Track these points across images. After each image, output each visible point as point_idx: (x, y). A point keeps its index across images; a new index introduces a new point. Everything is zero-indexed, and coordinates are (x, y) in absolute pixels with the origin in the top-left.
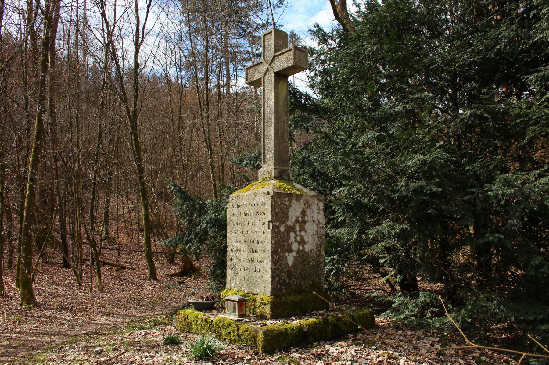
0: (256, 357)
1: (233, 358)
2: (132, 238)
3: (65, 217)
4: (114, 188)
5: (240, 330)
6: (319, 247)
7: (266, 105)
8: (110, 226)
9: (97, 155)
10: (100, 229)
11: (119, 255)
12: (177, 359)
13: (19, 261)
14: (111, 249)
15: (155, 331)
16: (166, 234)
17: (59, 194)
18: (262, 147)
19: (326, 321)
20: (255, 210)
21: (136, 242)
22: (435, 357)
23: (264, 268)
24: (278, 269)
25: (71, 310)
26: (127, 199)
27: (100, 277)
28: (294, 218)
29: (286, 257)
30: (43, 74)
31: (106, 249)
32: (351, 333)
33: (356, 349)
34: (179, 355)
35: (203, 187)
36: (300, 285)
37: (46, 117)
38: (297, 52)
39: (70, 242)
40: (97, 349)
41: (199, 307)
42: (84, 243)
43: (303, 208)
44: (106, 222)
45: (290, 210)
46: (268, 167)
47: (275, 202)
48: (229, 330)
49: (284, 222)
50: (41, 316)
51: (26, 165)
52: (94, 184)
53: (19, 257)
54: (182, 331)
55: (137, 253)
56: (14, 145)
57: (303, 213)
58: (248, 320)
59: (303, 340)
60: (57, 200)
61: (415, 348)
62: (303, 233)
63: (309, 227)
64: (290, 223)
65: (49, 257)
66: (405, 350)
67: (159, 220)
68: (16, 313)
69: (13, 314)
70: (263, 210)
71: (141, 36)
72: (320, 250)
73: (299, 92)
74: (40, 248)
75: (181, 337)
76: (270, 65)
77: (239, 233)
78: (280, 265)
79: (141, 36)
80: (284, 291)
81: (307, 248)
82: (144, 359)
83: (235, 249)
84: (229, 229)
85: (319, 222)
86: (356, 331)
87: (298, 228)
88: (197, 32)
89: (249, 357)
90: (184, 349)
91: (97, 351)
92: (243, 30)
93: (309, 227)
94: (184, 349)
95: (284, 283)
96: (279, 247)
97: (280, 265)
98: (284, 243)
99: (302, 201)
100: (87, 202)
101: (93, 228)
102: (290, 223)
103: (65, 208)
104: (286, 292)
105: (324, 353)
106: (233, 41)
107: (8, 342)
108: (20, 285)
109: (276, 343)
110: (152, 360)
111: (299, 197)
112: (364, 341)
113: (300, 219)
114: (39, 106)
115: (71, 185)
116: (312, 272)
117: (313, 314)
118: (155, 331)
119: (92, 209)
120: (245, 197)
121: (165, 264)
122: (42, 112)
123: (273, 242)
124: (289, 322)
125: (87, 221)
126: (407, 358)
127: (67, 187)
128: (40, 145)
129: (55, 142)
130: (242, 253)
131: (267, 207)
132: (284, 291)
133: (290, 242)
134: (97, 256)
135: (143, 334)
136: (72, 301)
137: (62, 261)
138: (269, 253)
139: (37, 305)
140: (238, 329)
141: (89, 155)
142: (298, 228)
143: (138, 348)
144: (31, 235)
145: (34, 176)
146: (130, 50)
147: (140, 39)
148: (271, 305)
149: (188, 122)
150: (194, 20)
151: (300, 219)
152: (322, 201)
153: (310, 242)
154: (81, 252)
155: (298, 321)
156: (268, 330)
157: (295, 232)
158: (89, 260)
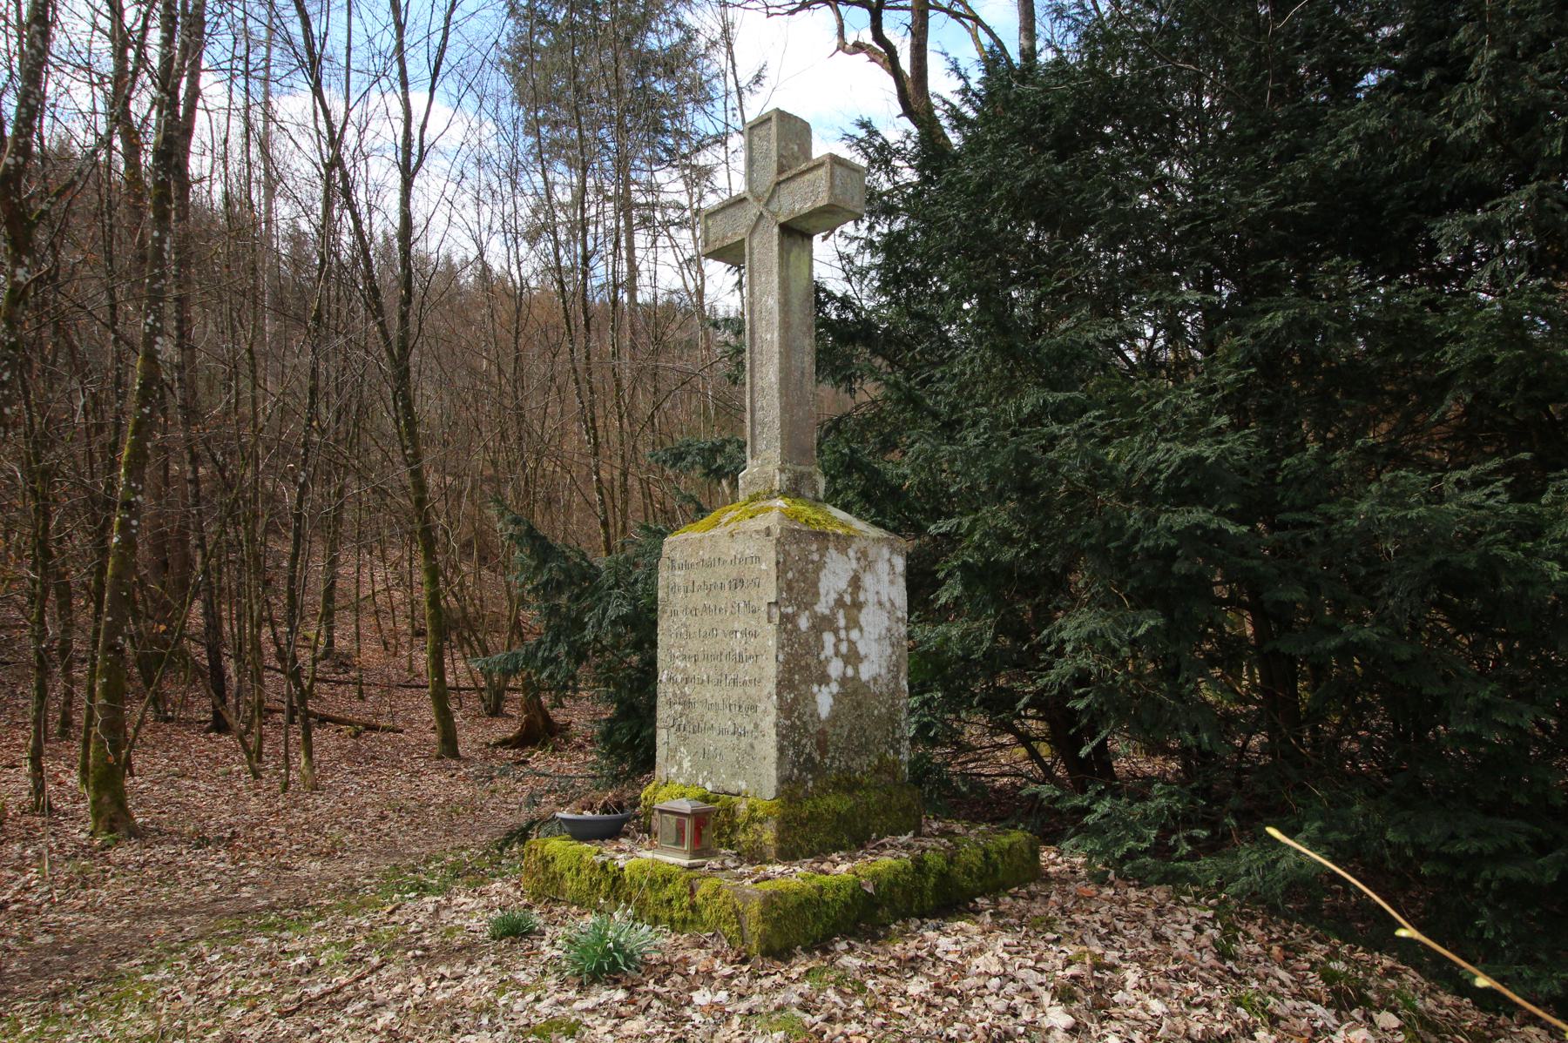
0: (745, 968)
1: (685, 976)
2: (395, 655)
3: (220, 603)
4: (347, 529)
5: (698, 894)
6: (894, 670)
7: (757, 308)
8: (336, 623)
9: (305, 445)
10: (312, 634)
11: (361, 697)
12: (529, 981)
13: (90, 717)
14: (339, 683)
15: (461, 899)
16: (482, 643)
17: (202, 546)
18: (748, 416)
19: (919, 865)
20: (735, 575)
21: (406, 665)
22: (1214, 962)
23: (756, 726)
24: (793, 727)
25: (229, 843)
26: (384, 559)
27: (309, 754)
28: (833, 596)
29: (813, 696)
30: (156, 234)
31: (326, 681)
32: (982, 895)
33: (1007, 941)
34: (532, 970)
35: (576, 530)
36: (849, 768)
37: (167, 348)
38: (838, 170)
39: (231, 667)
40: (302, 959)
41: (582, 832)
42: (270, 668)
43: (855, 571)
44: (328, 615)
45: (822, 575)
46: (764, 463)
47: (786, 554)
48: (668, 892)
49: (809, 606)
50: (146, 863)
51: (114, 466)
52: (299, 517)
53: (89, 708)
54: (538, 897)
55: (408, 692)
56: (79, 419)
57: (856, 583)
58: (717, 866)
59: (866, 916)
60: (199, 559)
61: (1158, 937)
62: (854, 634)
63: (870, 618)
64: (822, 608)
65: (174, 705)
66: (1132, 942)
67: (464, 609)
68: (75, 856)
69: (67, 859)
70: (754, 576)
71: (415, 150)
72: (896, 678)
73: (824, 290)
74: (148, 682)
75: (537, 918)
76: (767, 204)
77: (689, 635)
78: (799, 718)
79: (415, 150)
80: (810, 784)
81: (866, 672)
82: (435, 984)
83: (679, 677)
84: (663, 625)
85: (893, 604)
86: (995, 889)
87: (842, 622)
88: (557, 148)
89: (728, 970)
90: (548, 952)
91: (301, 965)
92: (667, 150)
93: (870, 618)
94: (548, 952)
95: (809, 765)
96: (799, 669)
97: (799, 718)
98: (809, 659)
99: (851, 553)
100: (278, 567)
101: (293, 630)
102: (822, 608)
103: (220, 579)
104: (815, 786)
105: (923, 953)
106: (644, 176)
107: (49, 939)
108: (91, 781)
109: (799, 931)
110: (459, 988)
111: (843, 542)
112: (1021, 918)
113: (848, 599)
114: (147, 316)
115: (236, 524)
116: (879, 734)
117: (883, 845)
118: (461, 899)
119: (292, 580)
120: (707, 543)
121: (480, 716)
122: (155, 332)
123: (781, 658)
124: (825, 867)
125: (279, 612)
126: (1142, 966)
127: (224, 525)
128: (151, 415)
129: (191, 413)
130: (698, 688)
131: (764, 567)
132: (810, 784)
133: (822, 657)
134: (303, 702)
135: (431, 908)
136: (233, 820)
137: (209, 716)
138: (770, 686)
139: (138, 833)
140: (692, 893)
141: (286, 449)
142: (842, 622)
143: (419, 953)
144: (123, 650)
145: (135, 494)
146: (390, 184)
147: (414, 160)
148: (779, 823)
149: (537, 368)
150: (545, 121)
151: (848, 599)
152: (900, 553)
153: (873, 657)
154: (260, 691)
155: (849, 865)
156: (775, 893)
157: (836, 632)
158: (282, 711)
